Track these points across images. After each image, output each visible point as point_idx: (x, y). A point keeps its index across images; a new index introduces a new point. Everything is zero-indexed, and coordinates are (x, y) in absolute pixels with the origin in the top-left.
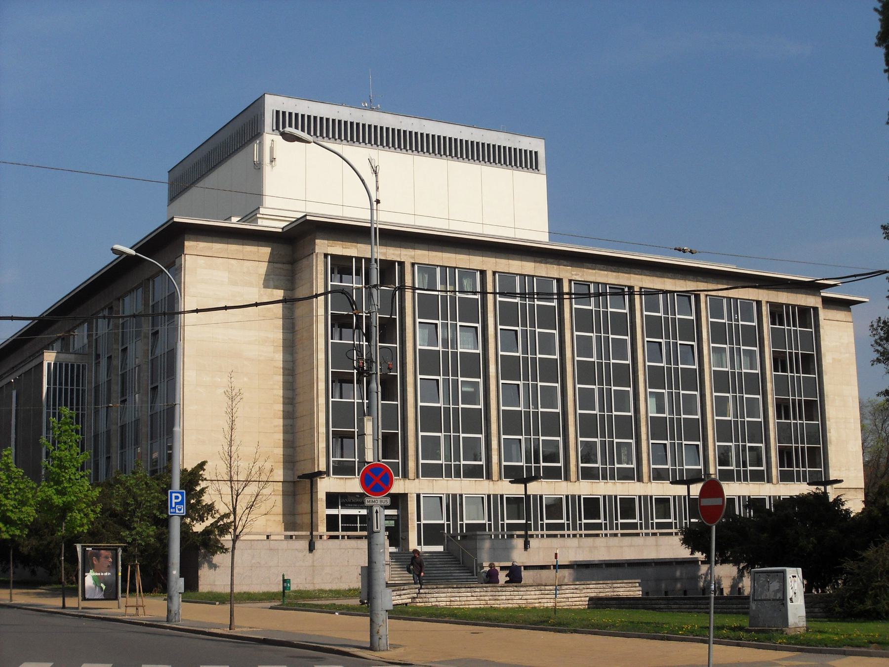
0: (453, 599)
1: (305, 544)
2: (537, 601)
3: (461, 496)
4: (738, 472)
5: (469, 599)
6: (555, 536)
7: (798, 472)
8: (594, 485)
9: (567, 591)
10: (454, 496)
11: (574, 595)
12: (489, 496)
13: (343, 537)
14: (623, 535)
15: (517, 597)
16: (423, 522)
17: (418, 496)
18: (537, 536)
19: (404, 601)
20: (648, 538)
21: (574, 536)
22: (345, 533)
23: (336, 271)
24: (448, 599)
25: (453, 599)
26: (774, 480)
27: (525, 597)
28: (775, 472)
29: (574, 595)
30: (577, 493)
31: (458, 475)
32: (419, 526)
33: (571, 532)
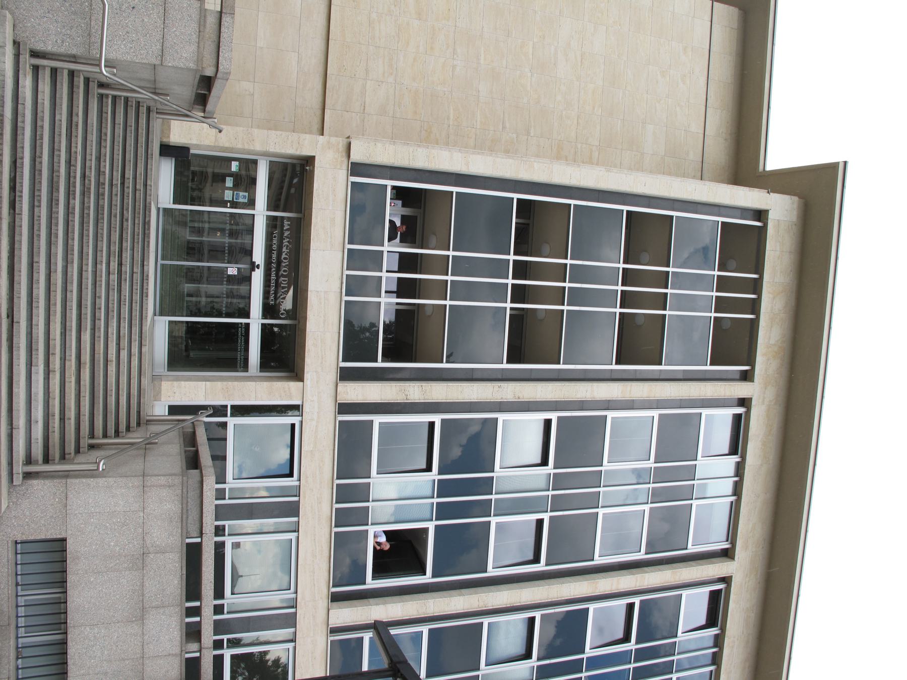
16: (232, 422)
17: (296, 408)
31: (342, 518)
33: (208, 619)
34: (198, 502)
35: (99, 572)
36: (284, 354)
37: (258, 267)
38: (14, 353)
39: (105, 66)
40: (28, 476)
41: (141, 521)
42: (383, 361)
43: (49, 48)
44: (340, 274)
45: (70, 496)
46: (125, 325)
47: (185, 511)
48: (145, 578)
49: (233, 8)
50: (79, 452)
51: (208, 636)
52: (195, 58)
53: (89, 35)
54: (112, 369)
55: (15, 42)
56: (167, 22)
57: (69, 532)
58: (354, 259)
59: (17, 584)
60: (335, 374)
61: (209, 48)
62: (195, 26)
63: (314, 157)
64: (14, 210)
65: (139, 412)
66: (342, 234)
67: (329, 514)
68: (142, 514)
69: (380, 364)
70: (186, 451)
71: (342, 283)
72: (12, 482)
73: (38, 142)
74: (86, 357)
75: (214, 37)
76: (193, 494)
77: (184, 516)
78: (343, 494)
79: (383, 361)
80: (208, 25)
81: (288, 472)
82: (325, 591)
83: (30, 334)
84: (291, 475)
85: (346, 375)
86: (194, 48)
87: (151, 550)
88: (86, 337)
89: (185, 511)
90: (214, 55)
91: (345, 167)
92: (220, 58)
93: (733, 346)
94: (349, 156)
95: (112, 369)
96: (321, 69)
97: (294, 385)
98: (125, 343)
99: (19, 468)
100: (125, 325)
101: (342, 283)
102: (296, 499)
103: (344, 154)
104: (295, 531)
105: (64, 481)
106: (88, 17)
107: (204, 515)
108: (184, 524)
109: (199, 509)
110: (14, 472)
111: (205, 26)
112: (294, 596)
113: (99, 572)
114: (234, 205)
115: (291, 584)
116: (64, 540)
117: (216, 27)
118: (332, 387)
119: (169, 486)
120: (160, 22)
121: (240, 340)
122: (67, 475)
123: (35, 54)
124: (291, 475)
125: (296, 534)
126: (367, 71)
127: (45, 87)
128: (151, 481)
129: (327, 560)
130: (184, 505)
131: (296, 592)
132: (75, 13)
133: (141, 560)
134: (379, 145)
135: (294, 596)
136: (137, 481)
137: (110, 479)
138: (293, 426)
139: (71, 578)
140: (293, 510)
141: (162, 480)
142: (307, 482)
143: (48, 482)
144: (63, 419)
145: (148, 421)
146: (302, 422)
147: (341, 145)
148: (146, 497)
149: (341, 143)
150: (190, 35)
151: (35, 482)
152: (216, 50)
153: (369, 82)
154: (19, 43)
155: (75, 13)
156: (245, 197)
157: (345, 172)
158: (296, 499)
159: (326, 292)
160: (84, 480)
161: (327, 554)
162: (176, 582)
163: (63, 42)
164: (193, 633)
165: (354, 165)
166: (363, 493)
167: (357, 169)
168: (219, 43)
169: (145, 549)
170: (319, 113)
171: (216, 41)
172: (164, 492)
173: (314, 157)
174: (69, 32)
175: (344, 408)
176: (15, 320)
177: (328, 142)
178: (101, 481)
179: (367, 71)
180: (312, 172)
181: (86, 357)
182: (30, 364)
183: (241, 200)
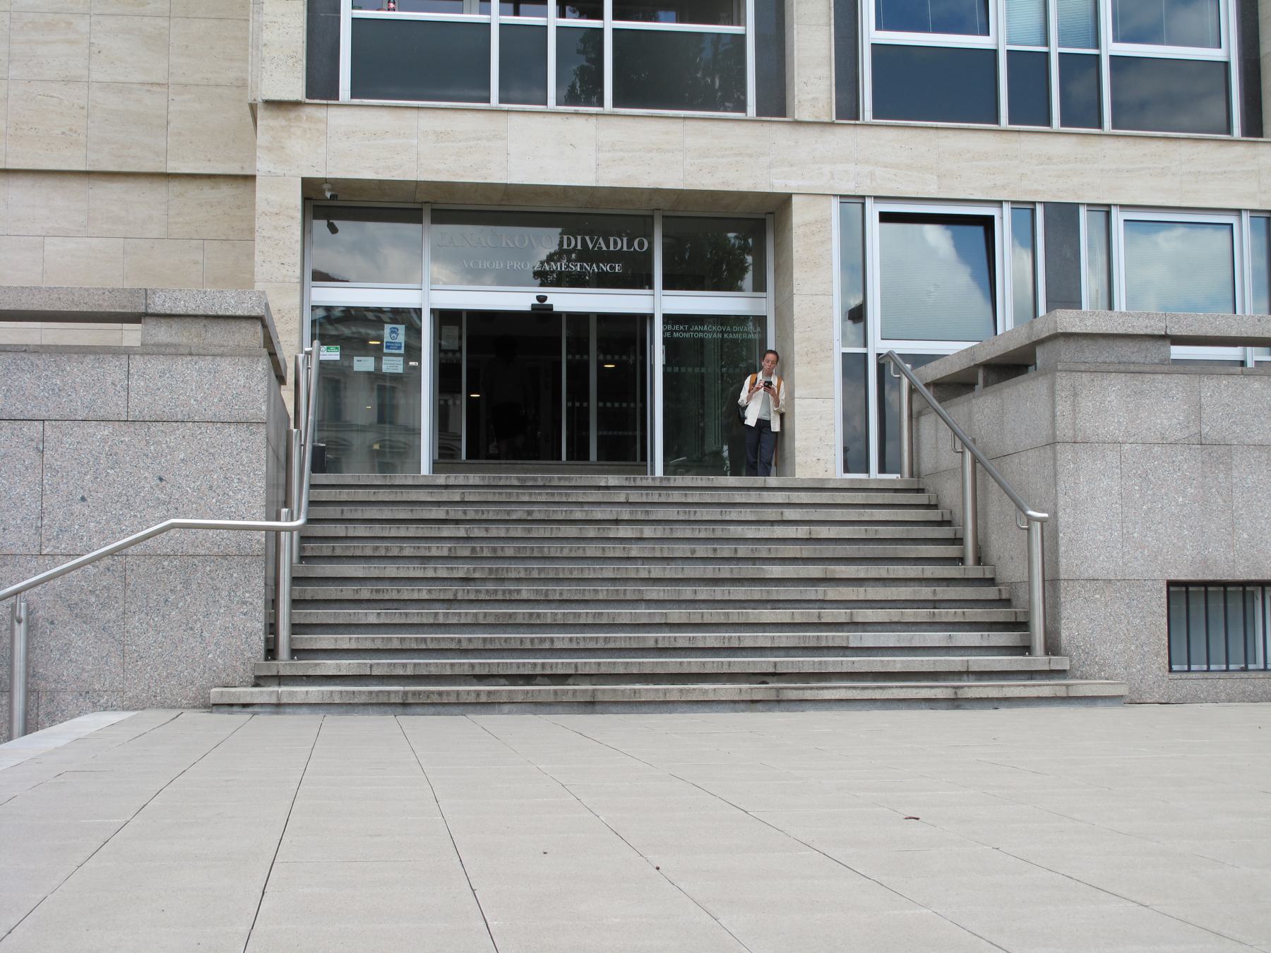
31: (1082, 114)
34: (1103, 342)
35: (1233, 524)
37: (542, 299)
38: (831, 670)
39: (292, 520)
40: (1052, 648)
41: (1140, 448)
42: (740, 21)
43: (258, 626)
44: (557, 119)
45: (1090, 573)
46: (734, 514)
47: (1122, 367)
48: (1247, 441)
49: (133, 292)
50: (992, 579)
52: (246, 361)
53: (225, 556)
54: (824, 532)
55: (256, 685)
56: (180, 417)
57: (1157, 574)
58: (523, 82)
59: (1245, 669)
60: (775, 127)
61: (217, 336)
62: (181, 365)
63: (307, 183)
64: (570, 675)
65: (896, 491)
66: (469, 115)
67: (1074, 139)
68: (1127, 447)
69: (749, 29)
70: (986, 385)
71: (576, 113)
72: (1064, 671)
73: (431, 646)
74: (815, 571)
75: (197, 327)
76: (1090, 352)
77: (1132, 368)
78: (1031, 111)
79: (740, 21)
80: (175, 340)
81: (979, 231)
82: (1240, 150)
83: (788, 651)
84: (987, 223)
85: (775, 103)
86: (225, 365)
87: (1194, 429)
88: (776, 571)
89: (1122, 367)
90: (234, 325)
91: (320, 113)
92: (239, 313)
94: (297, 104)
95: (824, 532)
96: (75, 185)
97: (800, 214)
98: (771, 514)
99: (1039, 660)
100: (734, 514)
101: (576, 113)
102: (1040, 211)
103: (292, 115)
104: (1108, 214)
105: (1063, 584)
106: (191, 560)
107: (1130, 331)
108: (1148, 369)
109: (1118, 343)
110: (1046, 668)
111: (175, 346)
112: (1246, 217)
113: (1233, 524)
114: (412, 351)
115: (1218, 219)
116: (1170, 584)
117: (175, 324)
118: (803, 132)
119: (1075, 395)
120: (182, 430)
121: (697, 332)
122: (1052, 583)
123: (271, 653)
124: (987, 223)
125: (1114, 211)
126: (66, 81)
127: (325, 641)
128: (1064, 429)
129: (1172, 146)
130: (1111, 368)
131: (1239, 211)
132: (186, 584)
133: (1212, 449)
134: (266, 36)
135: (1246, 217)
136: (1065, 454)
137: (1061, 502)
138: (885, 217)
139: (1241, 574)
140: (1063, 217)
141: (1063, 407)
142: (1004, 187)
143: (1066, 612)
144: (935, 604)
145: (912, 475)
146: (876, 197)
147: (272, 123)
148: (1094, 439)
149: (266, 120)
150: (200, 370)
151: (1064, 634)
152: (223, 324)
153: (96, 76)
154: (258, 677)
155: (186, 584)
156: (394, 331)
157: (333, 112)
158: (1040, 211)
159: (599, 149)
160: (1062, 549)
161: (1161, 144)
162: (1257, 385)
163: (245, 603)
165: (312, 91)
166: (1029, 67)
167: (321, 85)
168: (207, 317)
169: (1193, 440)
170: (176, 187)
171: (205, 322)
172: (1086, 405)
173: (307, 183)
174: (224, 593)
175: (848, 109)
176: (771, 670)
177: (269, 150)
178: (1064, 518)
179: (66, 81)
180: (335, 183)
181: (815, 571)
182: (845, 650)
183: (401, 338)
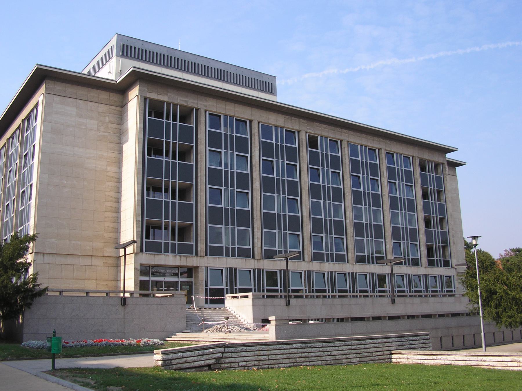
0: (261, 358)
1: (283, 301)
2: (344, 357)
3: (236, 269)
4: (166, 244)
5: (278, 357)
6: (343, 296)
7: (166, 244)
8: (322, 264)
9: (372, 346)
10: (231, 269)
11: (378, 349)
12: (254, 270)
13: (360, 296)
14: (339, 296)
15: (326, 353)
18: (311, 296)
19: (207, 362)
20: (325, 299)
21: (354, 296)
22: (361, 294)
23: (151, 190)
24: (256, 358)
25: (261, 358)
26: (424, 265)
27: (334, 353)
28: (201, 247)
29: (378, 349)
30: (261, 267)
32: (206, 289)
33: (331, 294)
36: (190, 271)
51: (334, 294)
84: (222, 270)
93: (186, 115)
164: (334, 297)
